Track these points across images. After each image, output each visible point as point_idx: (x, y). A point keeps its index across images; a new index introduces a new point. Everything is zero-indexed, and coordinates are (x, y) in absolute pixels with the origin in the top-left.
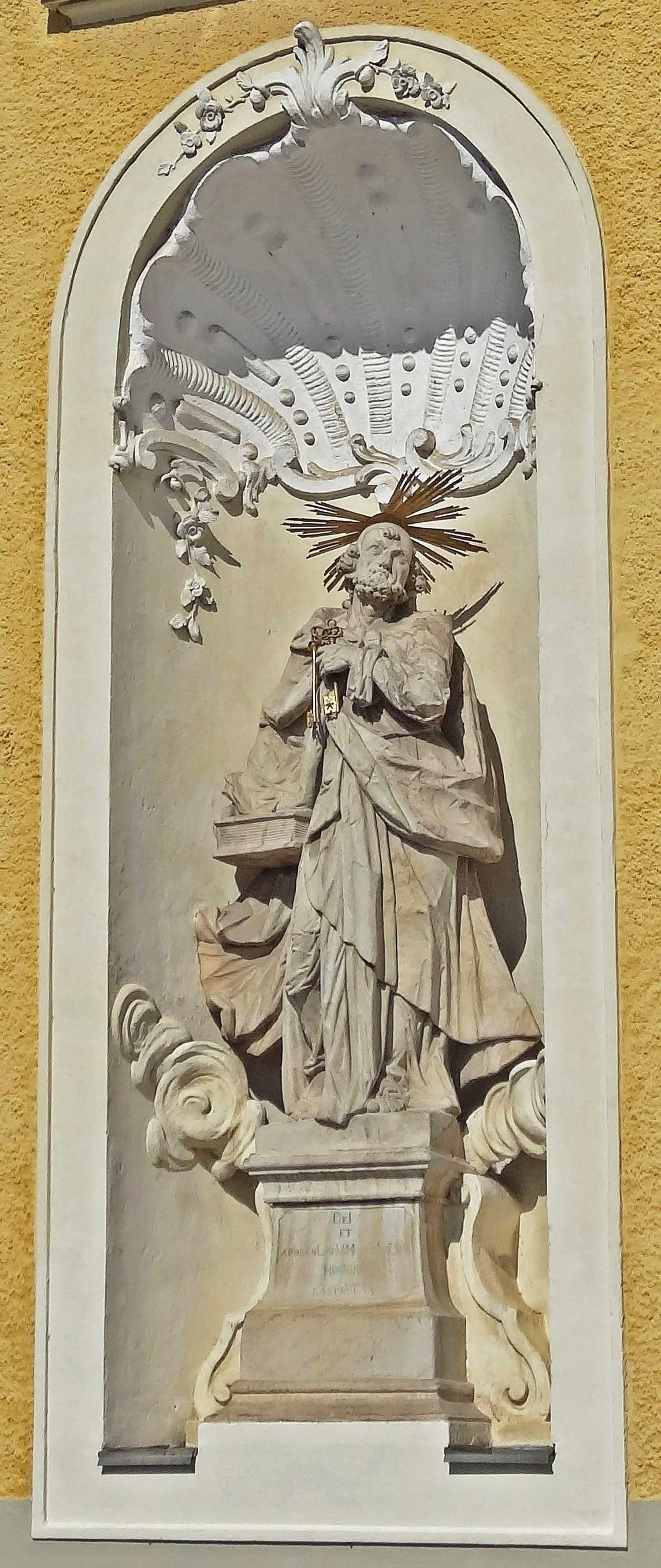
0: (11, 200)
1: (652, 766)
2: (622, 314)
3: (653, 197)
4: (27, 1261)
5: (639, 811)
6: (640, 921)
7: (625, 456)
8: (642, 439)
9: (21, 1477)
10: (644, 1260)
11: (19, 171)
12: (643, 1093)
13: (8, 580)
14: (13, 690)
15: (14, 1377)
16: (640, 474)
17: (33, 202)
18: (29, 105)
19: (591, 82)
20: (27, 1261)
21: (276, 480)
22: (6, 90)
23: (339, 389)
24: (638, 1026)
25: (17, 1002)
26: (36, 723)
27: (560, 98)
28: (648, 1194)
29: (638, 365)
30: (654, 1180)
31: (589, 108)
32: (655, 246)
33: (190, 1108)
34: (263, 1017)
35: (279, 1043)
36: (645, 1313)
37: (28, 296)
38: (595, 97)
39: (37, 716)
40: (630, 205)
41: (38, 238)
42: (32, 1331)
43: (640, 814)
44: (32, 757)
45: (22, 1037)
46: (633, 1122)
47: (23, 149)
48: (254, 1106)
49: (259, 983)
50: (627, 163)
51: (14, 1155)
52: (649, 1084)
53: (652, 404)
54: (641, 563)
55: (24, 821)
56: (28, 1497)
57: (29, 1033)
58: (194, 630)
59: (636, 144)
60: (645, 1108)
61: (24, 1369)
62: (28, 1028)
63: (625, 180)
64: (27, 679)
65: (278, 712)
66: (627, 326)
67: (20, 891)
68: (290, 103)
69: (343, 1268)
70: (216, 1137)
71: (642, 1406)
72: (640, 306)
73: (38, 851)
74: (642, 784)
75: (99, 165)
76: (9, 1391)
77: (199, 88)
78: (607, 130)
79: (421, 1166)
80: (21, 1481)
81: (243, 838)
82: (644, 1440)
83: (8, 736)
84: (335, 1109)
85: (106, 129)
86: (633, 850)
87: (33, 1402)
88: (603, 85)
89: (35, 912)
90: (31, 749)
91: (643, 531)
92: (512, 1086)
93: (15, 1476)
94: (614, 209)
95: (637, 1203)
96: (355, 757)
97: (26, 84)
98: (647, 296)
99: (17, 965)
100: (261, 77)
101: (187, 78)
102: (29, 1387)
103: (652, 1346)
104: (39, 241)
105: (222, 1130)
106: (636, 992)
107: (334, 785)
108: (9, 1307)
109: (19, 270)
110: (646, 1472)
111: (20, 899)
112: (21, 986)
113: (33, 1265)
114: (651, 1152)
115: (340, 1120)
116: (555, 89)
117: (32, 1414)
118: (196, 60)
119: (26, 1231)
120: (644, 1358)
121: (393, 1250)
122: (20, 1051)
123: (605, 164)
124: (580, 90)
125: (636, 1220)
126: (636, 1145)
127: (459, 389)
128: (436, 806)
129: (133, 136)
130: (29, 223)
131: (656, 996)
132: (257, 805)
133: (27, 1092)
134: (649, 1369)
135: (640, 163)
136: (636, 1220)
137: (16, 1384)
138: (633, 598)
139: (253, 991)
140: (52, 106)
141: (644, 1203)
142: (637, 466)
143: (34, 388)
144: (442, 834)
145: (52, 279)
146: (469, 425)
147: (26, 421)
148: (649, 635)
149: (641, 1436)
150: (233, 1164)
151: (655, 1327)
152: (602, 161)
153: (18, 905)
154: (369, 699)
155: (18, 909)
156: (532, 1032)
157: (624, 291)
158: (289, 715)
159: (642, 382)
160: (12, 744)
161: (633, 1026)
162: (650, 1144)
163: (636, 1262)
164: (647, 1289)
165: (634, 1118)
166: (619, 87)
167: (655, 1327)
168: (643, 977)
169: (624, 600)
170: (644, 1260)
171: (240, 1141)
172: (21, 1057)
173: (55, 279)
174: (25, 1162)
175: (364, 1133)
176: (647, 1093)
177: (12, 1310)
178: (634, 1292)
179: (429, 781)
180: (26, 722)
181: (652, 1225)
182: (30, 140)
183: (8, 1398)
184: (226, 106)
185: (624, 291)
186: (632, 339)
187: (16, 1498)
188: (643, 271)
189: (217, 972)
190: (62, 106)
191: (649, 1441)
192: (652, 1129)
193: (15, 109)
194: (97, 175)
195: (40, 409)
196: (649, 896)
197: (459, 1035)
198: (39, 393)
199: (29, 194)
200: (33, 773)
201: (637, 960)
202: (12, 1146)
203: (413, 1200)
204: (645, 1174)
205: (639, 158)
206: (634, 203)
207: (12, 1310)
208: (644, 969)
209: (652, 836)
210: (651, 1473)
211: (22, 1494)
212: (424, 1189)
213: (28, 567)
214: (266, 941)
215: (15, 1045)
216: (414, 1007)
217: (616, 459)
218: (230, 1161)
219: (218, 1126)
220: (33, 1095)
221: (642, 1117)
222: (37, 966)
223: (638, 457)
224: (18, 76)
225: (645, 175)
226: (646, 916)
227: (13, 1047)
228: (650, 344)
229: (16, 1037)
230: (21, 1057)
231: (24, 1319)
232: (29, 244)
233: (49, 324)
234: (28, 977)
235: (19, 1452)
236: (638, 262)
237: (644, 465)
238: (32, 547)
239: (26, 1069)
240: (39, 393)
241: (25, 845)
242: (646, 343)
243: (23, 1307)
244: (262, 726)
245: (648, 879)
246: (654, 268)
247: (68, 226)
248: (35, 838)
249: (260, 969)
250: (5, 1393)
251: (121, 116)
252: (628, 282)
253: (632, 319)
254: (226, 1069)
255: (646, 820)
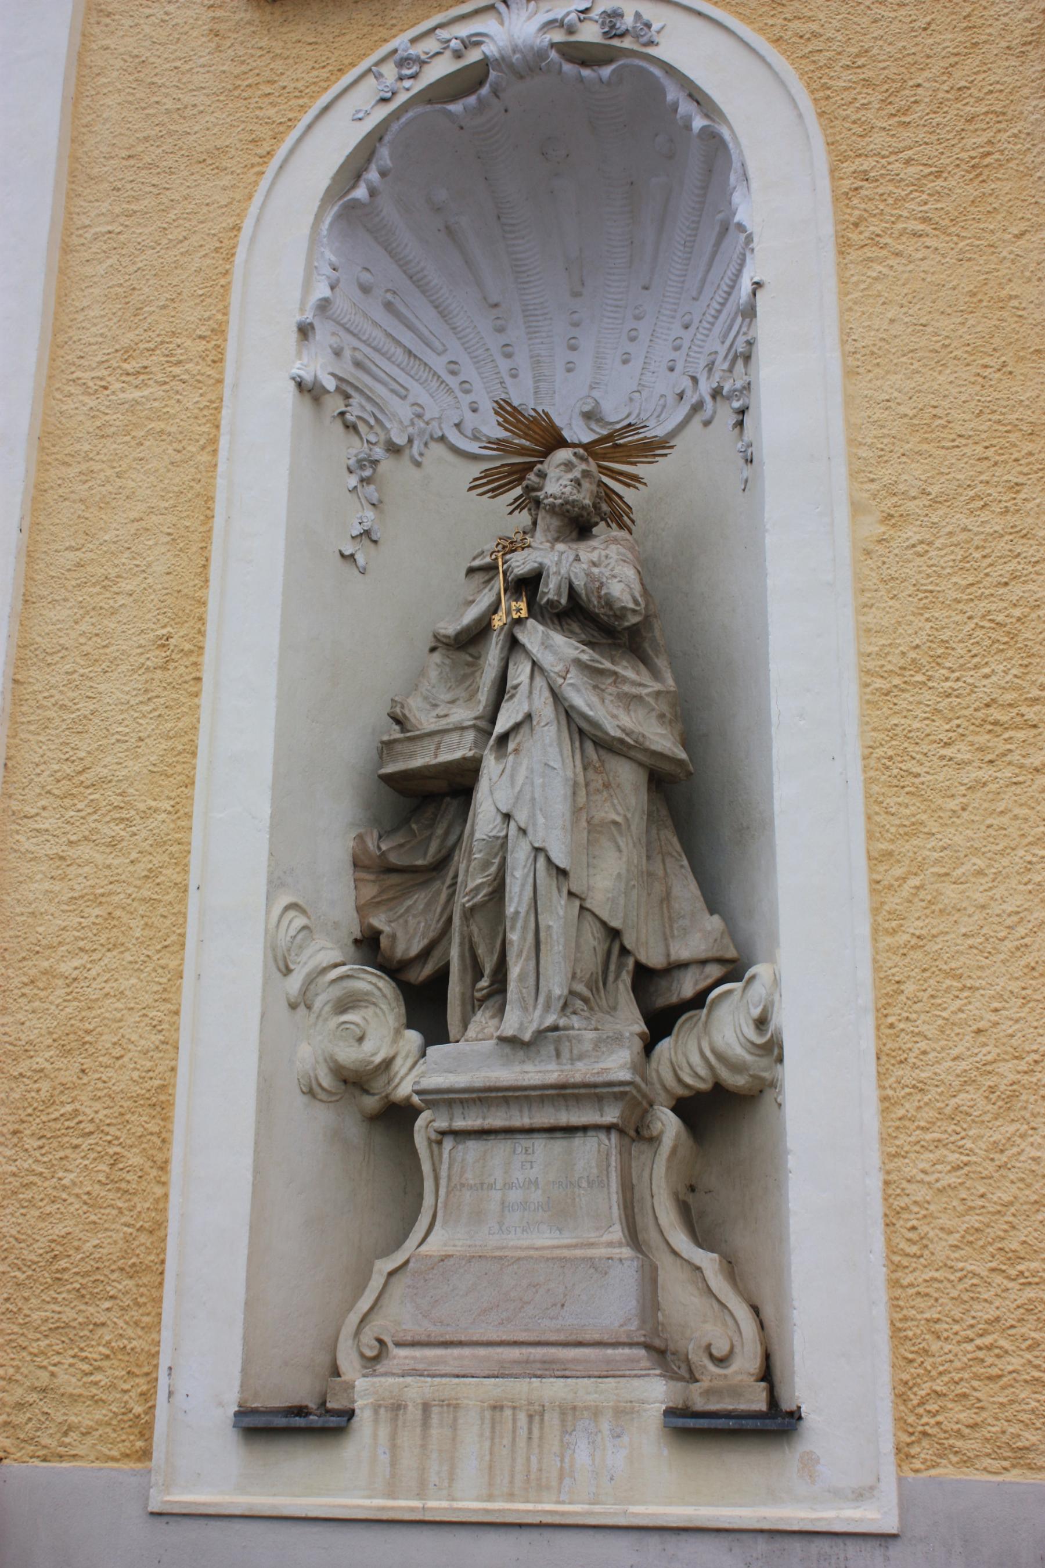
0: (199, 149)
1: (901, 648)
2: (850, 215)
3: (879, 109)
4: (159, 1191)
5: (886, 695)
6: (893, 810)
7: (859, 345)
8: (876, 327)
9: (139, 1440)
10: (910, 1188)
11: (210, 125)
12: (902, 998)
13: (176, 489)
14: (176, 594)
15: (136, 1323)
16: (875, 361)
17: (223, 150)
18: (224, 68)
19: (810, 14)
20: (159, 1191)
21: (442, 439)
22: (201, 57)
23: (504, 365)
24: (894, 924)
25: (162, 910)
26: (199, 625)
27: (777, 30)
28: (912, 1112)
29: (870, 260)
30: (918, 1097)
31: (808, 36)
32: (883, 153)
33: (344, 1034)
34: (426, 941)
35: (447, 966)
36: (914, 1249)
37: (213, 232)
38: (814, 26)
39: (201, 619)
40: (854, 117)
41: (226, 180)
42: (160, 1270)
43: (888, 698)
44: (193, 659)
45: (166, 947)
46: (891, 1031)
47: (214, 105)
48: (414, 1037)
49: (421, 907)
50: (850, 81)
51: (151, 1074)
52: (909, 988)
53: (886, 295)
54: (880, 446)
55: (180, 725)
56: (147, 1463)
57: (174, 943)
58: (360, 559)
59: (859, 63)
60: (905, 1015)
61: (148, 1314)
62: (174, 938)
63: (848, 96)
64: (191, 583)
65: (450, 628)
66: (856, 225)
67: (173, 795)
68: (489, 49)
69: (524, 1205)
70: (371, 1067)
71: (911, 1361)
72: (870, 206)
73: (194, 754)
74: (889, 667)
75: (291, 115)
76: (130, 1339)
77: (400, 41)
78: (827, 54)
79: (622, 1089)
80: (140, 1444)
81: (412, 756)
82: (915, 1402)
83: (167, 639)
84: (522, 1027)
85: (300, 85)
86: (883, 736)
87: (158, 1353)
88: (821, 16)
89: (189, 816)
90: (192, 652)
91: (878, 414)
92: (745, 988)
93: (132, 1438)
94: (837, 122)
95: (898, 1123)
96: (547, 660)
97: (220, 51)
98: (877, 197)
99: (164, 872)
100: (464, 30)
101: (386, 37)
102: (154, 1336)
103: (922, 1289)
104: (227, 183)
105: (378, 1059)
106: (890, 887)
107: (524, 689)
108: (136, 1243)
109: (205, 209)
110: (919, 1441)
111: (172, 803)
112: (168, 893)
113: (166, 1195)
114: (914, 1064)
115: (527, 1037)
116: (770, 22)
117: (156, 1366)
118: (394, 21)
119: (159, 1157)
120: (912, 1303)
121: (584, 1184)
122: (162, 962)
123: (826, 83)
124: (797, 22)
125: (898, 1142)
126: (894, 1057)
127: (625, 362)
128: (632, 713)
129: (326, 89)
130: (217, 168)
131: (913, 891)
132: (425, 720)
133: (169, 1006)
134: (919, 1317)
135: (864, 80)
136: (898, 1142)
137: (140, 1332)
138: (872, 481)
139: (414, 916)
140: (244, 68)
141: (907, 1123)
142: (872, 353)
143: (214, 312)
144: (641, 739)
145: (238, 215)
146: (638, 391)
147: (204, 342)
148: (892, 516)
149: (912, 1396)
150: (387, 1096)
151: (925, 1267)
152: (822, 81)
153: (170, 809)
154: (564, 601)
155: (170, 813)
156: (731, 953)
157: (851, 194)
158: (467, 630)
159: (874, 274)
160: (172, 648)
161: (887, 925)
162: (912, 1055)
163: (898, 1191)
164: (915, 1223)
165: (891, 1026)
166: (839, 17)
167: (925, 1267)
168: (898, 871)
169: (862, 483)
170: (910, 1188)
171: (397, 1073)
172: (163, 968)
173: (241, 215)
174: (162, 1082)
175: (554, 1053)
176: (908, 998)
177: (138, 1246)
178: (898, 1226)
179: (626, 688)
180: (187, 625)
181: (917, 1148)
182: (221, 98)
183: (129, 1347)
184: (423, 57)
185: (851, 194)
186: (862, 237)
187: (132, 1465)
188: (872, 174)
189: (374, 897)
190: (255, 68)
191: (921, 1404)
192: (915, 1039)
193: (208, 72)
194: (290, 124)
195: (220, 331)
196: (902, 784)
197: (648, 958)
198: (219, 317)
199: (219, 143)
200: (194, 675)
201: (890, 854)
202: (149, 1064)
203: (608, 1128)
204: (907, 1090)
205: (862, 76)
206: (859, 116)
207: (138, 1246)
208: (899, 861)
209: (903, 721)
210: (925, 1443)
211: (139, 1460)
212: (621, 1117)
213: (199, 476)
214: (431, 864)
215: (158, 956)
216: (604, 924)
217: (849, 348)
218: (384, 1094)
219: (373, 1055)
220: (173, 1008)
221: (902, 1025)
222: (187, 872)
223: (874, 345)
224: (213, 45)
225: (870, 91)
226: (900, 804)
227: (155, 958)
228: (883, 241)
229: (159, 947)
230: (163, 968)
231: (152, 1257)
232: (216, 186)
233: (233, 255)
234: (176, 884)
235: (138, 1409)
236: (865, 167)
237: (880, 353)
238: (204, 457)
239: (169, 980)
240: (219, 317)
241: (180, 747)
242: (877, 239)
243: (152, 1243)
244: (433, 650)
245: (900, 765)
246: (883, 172)
247: (257, 169)
248: (192, 740)
249: (423, 895)
250: (126, 1342)
251: (315, 73)
252: (855, 185)
253: (861, 218)
254: (385, 996)
255: (895, 704)
